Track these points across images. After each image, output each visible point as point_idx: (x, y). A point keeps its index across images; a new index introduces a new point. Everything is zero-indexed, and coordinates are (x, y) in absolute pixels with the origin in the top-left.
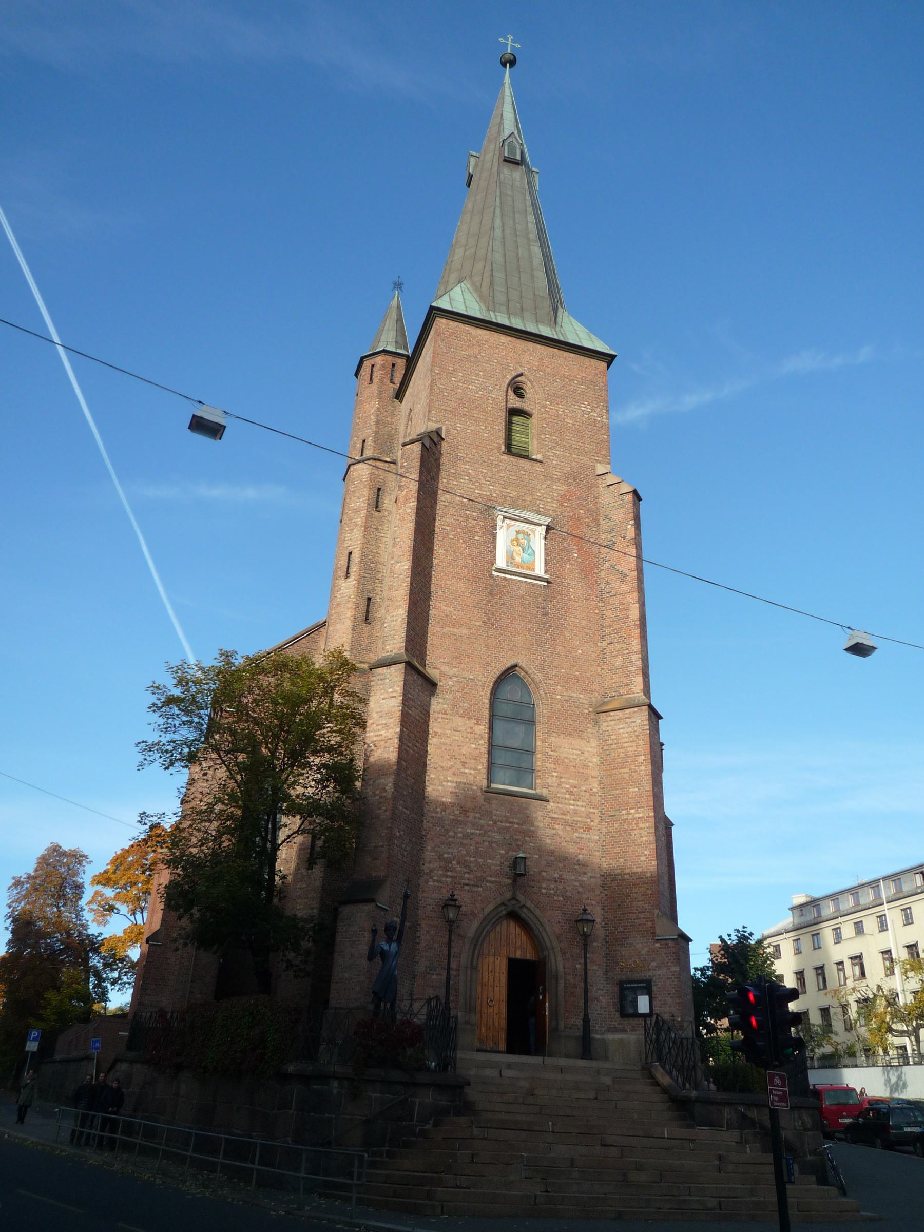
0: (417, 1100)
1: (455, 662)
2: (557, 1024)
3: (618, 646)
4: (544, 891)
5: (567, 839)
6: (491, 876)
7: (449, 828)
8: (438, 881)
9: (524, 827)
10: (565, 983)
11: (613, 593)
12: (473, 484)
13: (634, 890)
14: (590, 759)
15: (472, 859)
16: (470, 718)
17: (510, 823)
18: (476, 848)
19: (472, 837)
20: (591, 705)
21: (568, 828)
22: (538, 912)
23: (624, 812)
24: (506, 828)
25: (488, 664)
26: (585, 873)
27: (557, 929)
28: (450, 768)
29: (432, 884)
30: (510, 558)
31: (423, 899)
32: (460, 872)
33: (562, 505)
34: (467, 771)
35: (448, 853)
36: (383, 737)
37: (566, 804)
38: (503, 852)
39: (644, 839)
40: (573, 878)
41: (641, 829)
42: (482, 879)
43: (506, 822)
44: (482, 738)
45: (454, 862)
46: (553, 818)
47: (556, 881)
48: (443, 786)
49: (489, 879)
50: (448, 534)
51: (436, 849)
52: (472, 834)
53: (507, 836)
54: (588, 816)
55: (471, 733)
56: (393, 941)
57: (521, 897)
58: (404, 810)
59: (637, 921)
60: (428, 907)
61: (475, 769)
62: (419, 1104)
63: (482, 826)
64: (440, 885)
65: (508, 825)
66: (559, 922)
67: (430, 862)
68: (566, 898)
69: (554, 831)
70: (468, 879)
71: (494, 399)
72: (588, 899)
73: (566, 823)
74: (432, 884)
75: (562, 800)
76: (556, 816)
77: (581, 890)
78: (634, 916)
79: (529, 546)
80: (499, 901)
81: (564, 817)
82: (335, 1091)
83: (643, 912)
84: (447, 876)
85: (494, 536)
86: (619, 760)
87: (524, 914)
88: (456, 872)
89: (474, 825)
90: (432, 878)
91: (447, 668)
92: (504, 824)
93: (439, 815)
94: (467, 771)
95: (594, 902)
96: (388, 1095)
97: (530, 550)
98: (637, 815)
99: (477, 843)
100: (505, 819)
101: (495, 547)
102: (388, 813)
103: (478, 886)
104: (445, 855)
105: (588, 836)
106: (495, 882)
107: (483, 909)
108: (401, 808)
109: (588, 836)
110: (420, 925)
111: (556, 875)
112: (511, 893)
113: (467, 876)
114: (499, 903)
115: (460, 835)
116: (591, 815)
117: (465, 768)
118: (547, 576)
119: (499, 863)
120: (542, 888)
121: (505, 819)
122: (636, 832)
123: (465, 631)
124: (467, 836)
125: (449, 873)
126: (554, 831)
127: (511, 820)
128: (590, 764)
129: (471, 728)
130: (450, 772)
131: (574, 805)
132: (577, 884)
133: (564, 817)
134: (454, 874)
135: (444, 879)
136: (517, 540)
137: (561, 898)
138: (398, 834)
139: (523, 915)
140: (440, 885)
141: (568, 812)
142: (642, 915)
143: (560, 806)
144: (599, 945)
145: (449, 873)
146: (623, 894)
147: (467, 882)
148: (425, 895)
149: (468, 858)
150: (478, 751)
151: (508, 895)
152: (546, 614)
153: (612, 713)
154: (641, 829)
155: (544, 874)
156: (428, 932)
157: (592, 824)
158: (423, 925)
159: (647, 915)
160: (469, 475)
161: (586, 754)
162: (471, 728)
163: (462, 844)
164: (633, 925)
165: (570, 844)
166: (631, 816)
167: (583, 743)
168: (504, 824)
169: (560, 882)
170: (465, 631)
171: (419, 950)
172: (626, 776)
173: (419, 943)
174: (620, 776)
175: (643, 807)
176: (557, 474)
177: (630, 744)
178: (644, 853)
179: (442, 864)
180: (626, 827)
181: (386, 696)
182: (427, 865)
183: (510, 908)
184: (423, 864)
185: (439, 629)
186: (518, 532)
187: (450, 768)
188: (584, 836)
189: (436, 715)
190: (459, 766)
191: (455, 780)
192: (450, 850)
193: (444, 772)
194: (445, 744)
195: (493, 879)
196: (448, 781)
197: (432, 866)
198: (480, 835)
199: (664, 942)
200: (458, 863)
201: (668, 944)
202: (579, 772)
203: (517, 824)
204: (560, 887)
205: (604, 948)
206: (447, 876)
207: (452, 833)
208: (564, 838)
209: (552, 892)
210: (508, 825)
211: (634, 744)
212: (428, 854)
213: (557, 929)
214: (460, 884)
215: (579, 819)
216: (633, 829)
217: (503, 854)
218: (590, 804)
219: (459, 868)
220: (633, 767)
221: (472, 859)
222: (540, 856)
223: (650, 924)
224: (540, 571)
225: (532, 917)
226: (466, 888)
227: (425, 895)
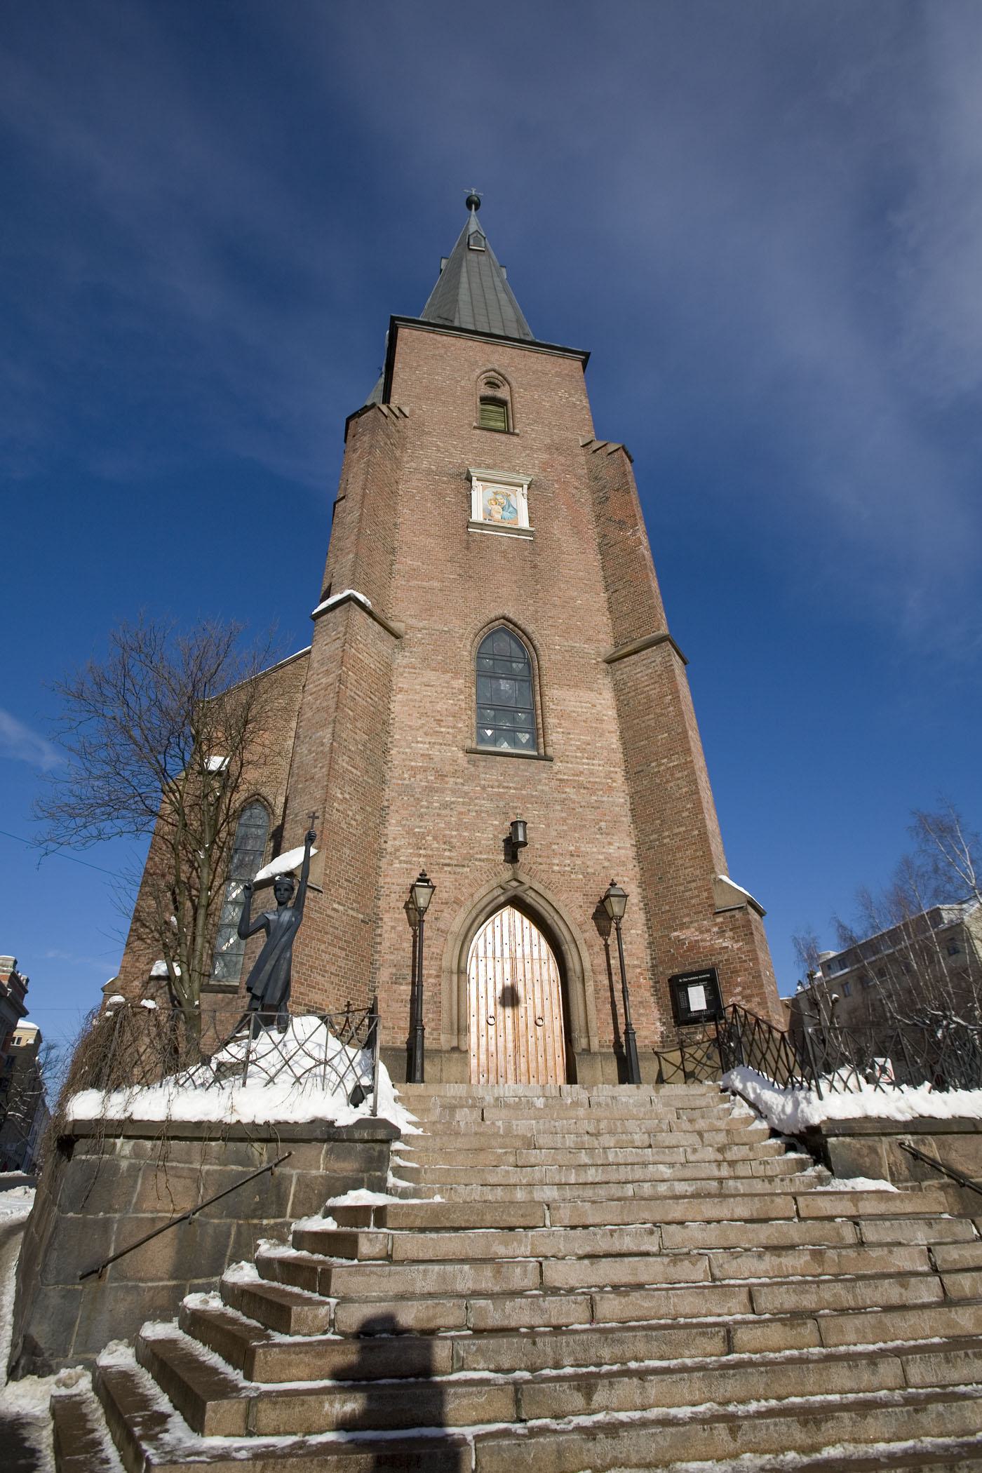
0: (294, 1172)
1: (424, 615)
2: (589, 1044)
3: (624, 592)
4: (556, 868)
5: (583, 804)
6: (481, 853)
7: (420, 796)
8: (406, 862)
9: (524, 792)
10: (596, 986)
11: (612, 543)
12: (442, 453)
13: (679, 855)
14: (604, 712)
15: (454, 833)
16: (446, 672)
17: (503, 787)
18: (460, 819)
19: (453, 806)
20: (599, 655)
21: (582, 791)
22: (549, 895)
23: (654, 764)
24: (499, 794)
25: (466, 616)
26: (610, 844)
27: (578, 916)
28: (421, 727)
29: (398, 866)
30: (488, 513)
31: (386, 886)
32: (438, 849)
33: (545, 471)
34: (443, 730)
35: (420, 827)
36: (323, 686)
37: (577, 763)
38: (497, 823)
39: (684, 790)
40: (595, 850)
41: (679, 779)
42: (470, 857)
43: (498, 787)
44: (462, 692)
45: (429, 838)
46: (560, 780)
47: (572, 855)
48: (411, 748)
49: (478, 856)
50: (414, 496)
51: (404, 822)
52: (453, 803)
53: (502, 804)
54: (608, 776)
55: (447, 688)
56: (286, 908)
57: (524, 878)
58: (350, 768)
59: (687, 894)
60: (393, 895)
61: (454, 727)
62: (298, 1179)
63: (466, 793)
64: (409, 866)
65: (501, 790)
66: (581, 907)
67: (395, 839)
68: (586, 874)
69: (564, 796)
70: (450, 858)
71: (461, 387)
72: (617, 875)
73: (581, 786)
74: (398, 866)
75: (573, 760)
76: (566, 777)
77: (606, 864)
78: (682, 888)
79: (510, 505)
80: (494, 883)
81: (577, 778)
82: (124, 1164)
83: (694, 881)
84: (420, 855)
85: (469, 497)
86: (641, 708)
87: (531, 898)
88: (432, 850)
89: (454, 792)
90: (397, 858)
91: (414, 620)
92: (496, 790)
93: (406, 782)
94: (443, 730)
95: (626, 879)
96: (233, 1167)
97: (511, 509)
98: (671, 764)
99: (461, 813)
100: (496, 784)
101: (470, 507)
102: (324, 770)
103: (464, 866)
104: (417, 830)
105: (611, 799)
106: (487, 860)
107: (472, 895)
108: (344, 764)
109: (611, 799)
110: (381, 919)
111: (572, 848)
112: (510, 873)
113: (447, 853)
114: (495, 885)
115: (435, 804)
116: (612, 775)
117: (441, 726)
118: (532, 529)
119: (491, 836)
120: (554, 864)
121: (496, 784)
122: (672, 784)
123: (436, 584)
124: (446, 806)
125: (422, 852)
126: (564, 796)
127: (505, 784)
128: (605, 718)
129: (448, 683)
130: (421, 732)
131: (588, 764)
132: (601, 857)
133: (577, 778)
134: (430, 852)
135: (415, 859)
136: (496, 500)
137: (581, 876)
138: (340, 796)
139: (529, 900)
140: (409, 866)
141: (582, 773)
142: (693, 885)
143: (570, 765)
144: (639, 932)
145: (422, 852)
146: (664, 863)
147: (447, 861)
148: (388, 880)
149: (448, 832)
150: (457, 708)
151: (507, 875)
152: (535, 567)
153: (625, 660)
154: (679, 779)
155: (555, 847)
156: (393, 928)
157: (614, 784)
158: (385, 920)
159: (699, 883)
160: (437, 446)
161: (599, 708)
162: (448, 683)
163: (439, 815)
164: (682, 900)
165: (587, 809)
166: (663, 768)
167: (593, 695)
168: (496, 790)
169: (578, 856)
170: (436, 584)
171: (380, 952)
172: (652, 723)
173: (380, 943)
174: (643, 725)
175: (677, 753)
176: (536, 445)
177: (652, 687)
178: (685, 807)
179: (413, 840)
180: (658, 781)
181: (328, 641)
182: (390, 843)
183: (510, 894)
184: (385, 842)
185: (403, 583)
186: (496, 493)
187: (421, 727)
188: (605, 799)
189: (401, 670)
190: (434, 724)
191: (427, 740)
192: (422, 824)
193: (413, 732)
194: (412, 700)
195: (485, 857)
196: (418, 742)
197: (397, 843)
198: (463, 803)
199: (728, 914)
200: (435, 838)
201: (734, 916)
202: (591, 727)
203: (515, 789)
204: (578, 861)
205: (647, 936)
206: (420, 855)
207: (425, 803)
208: (579, 803)
209: (567, 869)
210: (501, 790)
211: (657, 685)
212: (393, 828)
213: (578, 916)
214: (438, 864)
215: (597, 780)
216: (668, 782)
217: (496, 825)
218: (609, 762)
219: (435, 845)
220: (658, 711)
221: (454, 833)
222: (548, 826)
223: (705, 894)
224: (524, 523)
225: (556, 917)
226: (446, 868)
227: (388, 880)
